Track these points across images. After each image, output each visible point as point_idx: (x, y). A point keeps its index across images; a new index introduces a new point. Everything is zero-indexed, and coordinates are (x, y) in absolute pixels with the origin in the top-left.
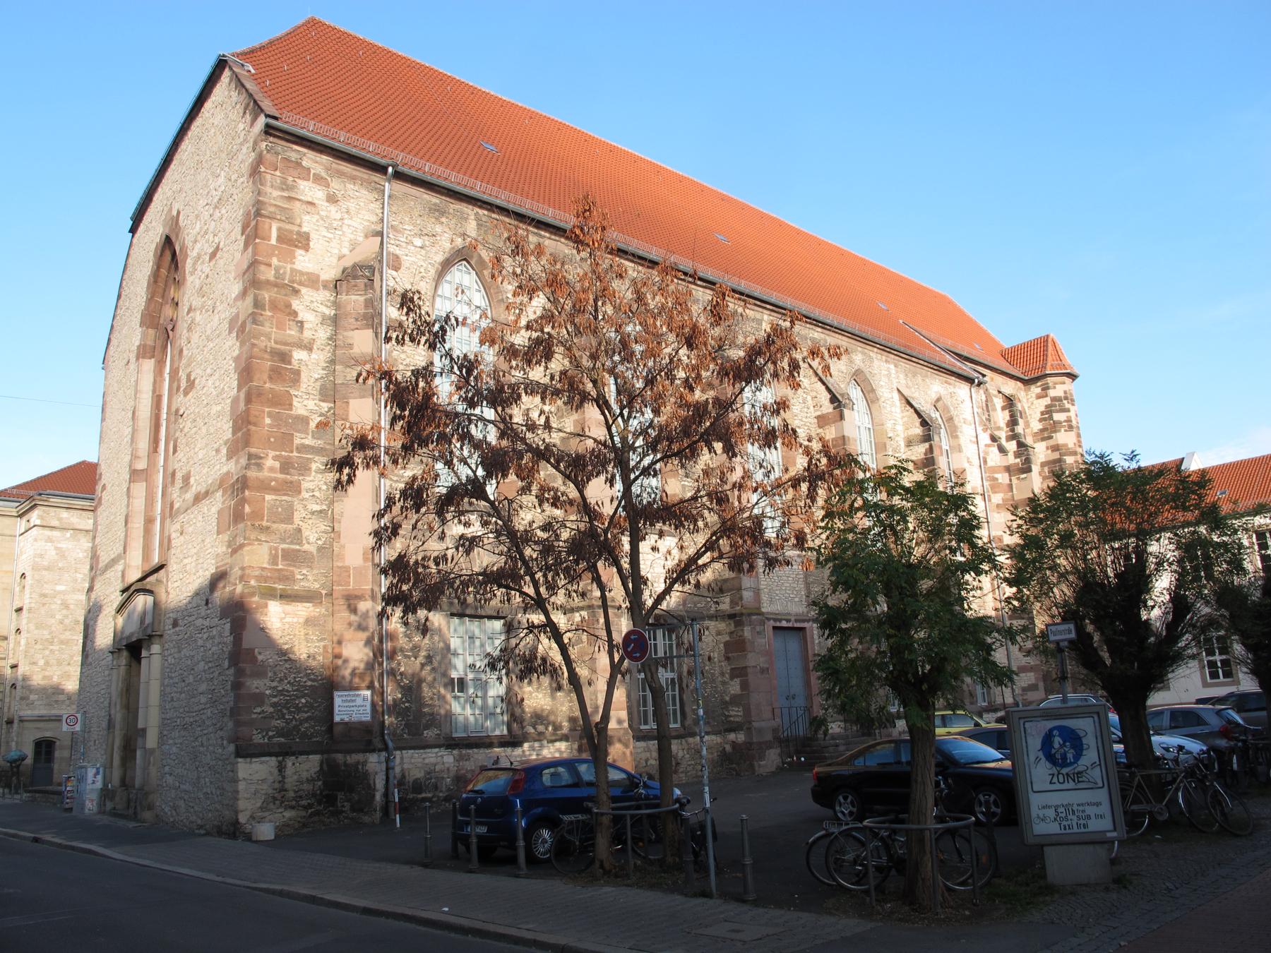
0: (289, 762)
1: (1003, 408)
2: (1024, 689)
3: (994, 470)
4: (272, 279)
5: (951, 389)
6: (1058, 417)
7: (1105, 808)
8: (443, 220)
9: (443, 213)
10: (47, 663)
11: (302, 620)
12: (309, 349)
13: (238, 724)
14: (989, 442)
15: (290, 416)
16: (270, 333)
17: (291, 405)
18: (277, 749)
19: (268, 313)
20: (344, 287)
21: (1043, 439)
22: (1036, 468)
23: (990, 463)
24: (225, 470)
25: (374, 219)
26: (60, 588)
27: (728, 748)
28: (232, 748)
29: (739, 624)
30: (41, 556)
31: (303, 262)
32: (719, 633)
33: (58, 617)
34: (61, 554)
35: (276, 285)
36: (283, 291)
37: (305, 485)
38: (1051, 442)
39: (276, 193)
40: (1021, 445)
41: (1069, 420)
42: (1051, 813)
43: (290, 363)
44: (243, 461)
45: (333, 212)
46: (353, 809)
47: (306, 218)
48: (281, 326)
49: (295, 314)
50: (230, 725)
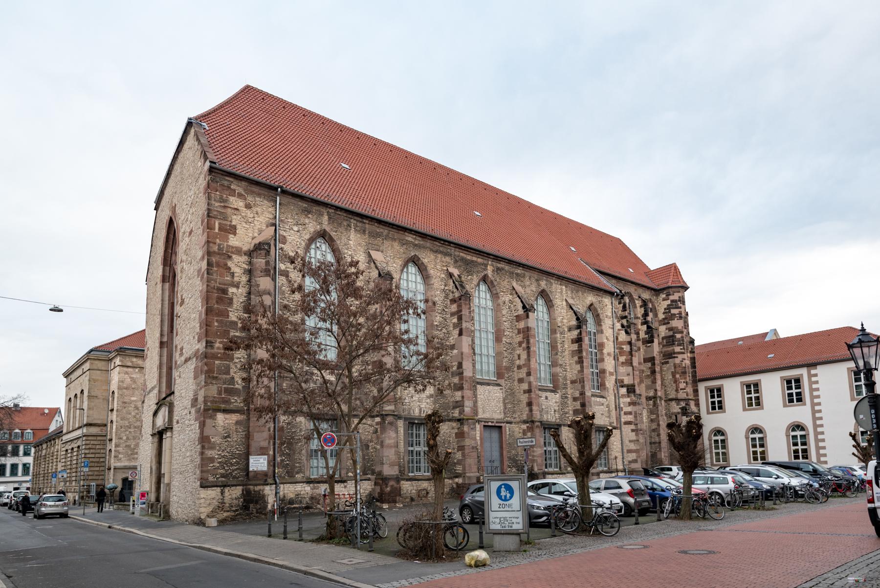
0: (226, 490)
1: (641, 307)
2: (630, 462)
3: (622, 343)
5: (600, 299)
6: (674, 311)
7: (520, 520)
9: (309, 212)
10: (128, 438)
13: (202, 472)
14: (620, 327)
21: (664, 324)
22: (656, 341)
23: (620, 339)
25: (271, 216)
26: (133, 399)
27: (455, 486)
28: (199, 483)
29: (462, 424)
30: (122, 382)
31: (233, 241)
32: (453, 428)
33: (133, 414)
37: (236, 356)
38: (669, 326)
39: (217, 204)
40: (649, 327)
41: (680, 313)
42: (498, 521)
44: (204, 344)
45: (249, 214)
46: (257, 512)
48: (222, 275)
49: (230, 268)
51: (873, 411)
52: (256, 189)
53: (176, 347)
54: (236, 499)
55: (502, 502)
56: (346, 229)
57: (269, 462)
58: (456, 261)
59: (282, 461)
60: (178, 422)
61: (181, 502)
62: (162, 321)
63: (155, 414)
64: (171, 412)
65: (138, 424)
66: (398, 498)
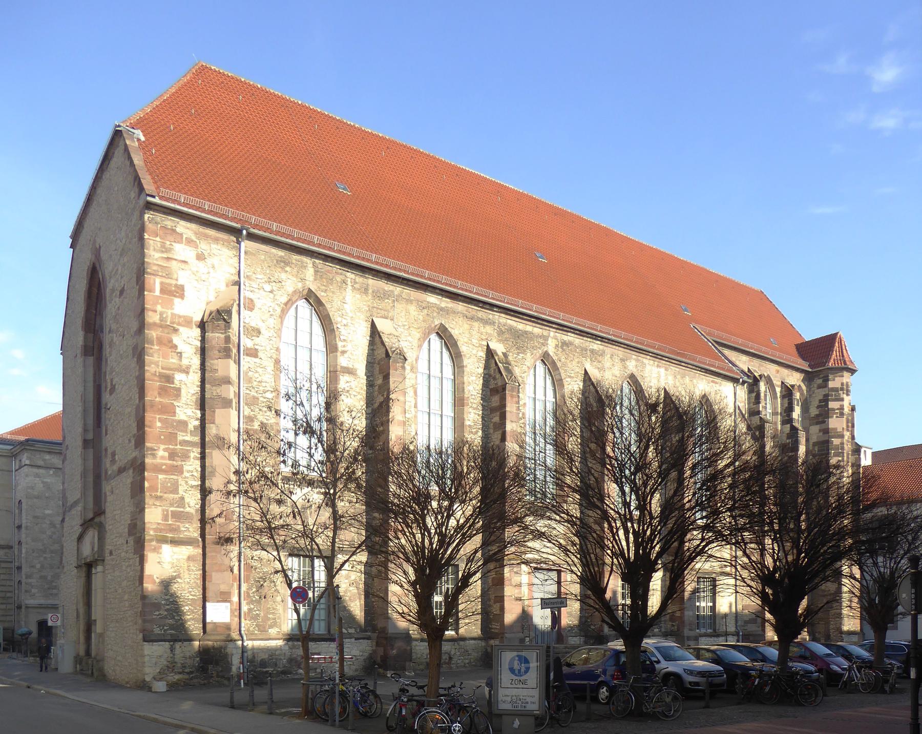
0: (178, 645)
4: (158, 321)
5: (716, 387)
8: (288, 269)
9: (287, 263)
10: (42, 567)
11: (185, 557)
12: (187, 373)
13: (144, 621)
14: (744, 430)
15: (175, 421)
16: (158, 362)
17: (175, 413)
18: (169, 637)
19: (156, 347)
20: (210, 327)
21: (817, 423)
24: (134, 455)
26: (47, 512)
28: (141, 636)
30: (32, 488)
33: (49, 533)
34: (47, 486)
35: (161, 326)
36: (166, 331)
37: (186, 468)
38: (823, 426)
39: (158, 255)
43: (173, 383)
46: (218, 676)
47: (181, 273)
48: (165, 356)
49: (176, 347)
50: (140, 621)
51: (913, 591)
52: (212, 232)
53: (106, 450)
54: (190, 658)
55: (515, 678)
56: (340, 287)
57: (232, 611)
58: (501, 333)
59: (250, 610)
60: (111, 553)
61: (119, 658)
62: (85, 411)
63: (80, 538)
64: (101, 539)
65: (56, 547)
66: (407, 664)
